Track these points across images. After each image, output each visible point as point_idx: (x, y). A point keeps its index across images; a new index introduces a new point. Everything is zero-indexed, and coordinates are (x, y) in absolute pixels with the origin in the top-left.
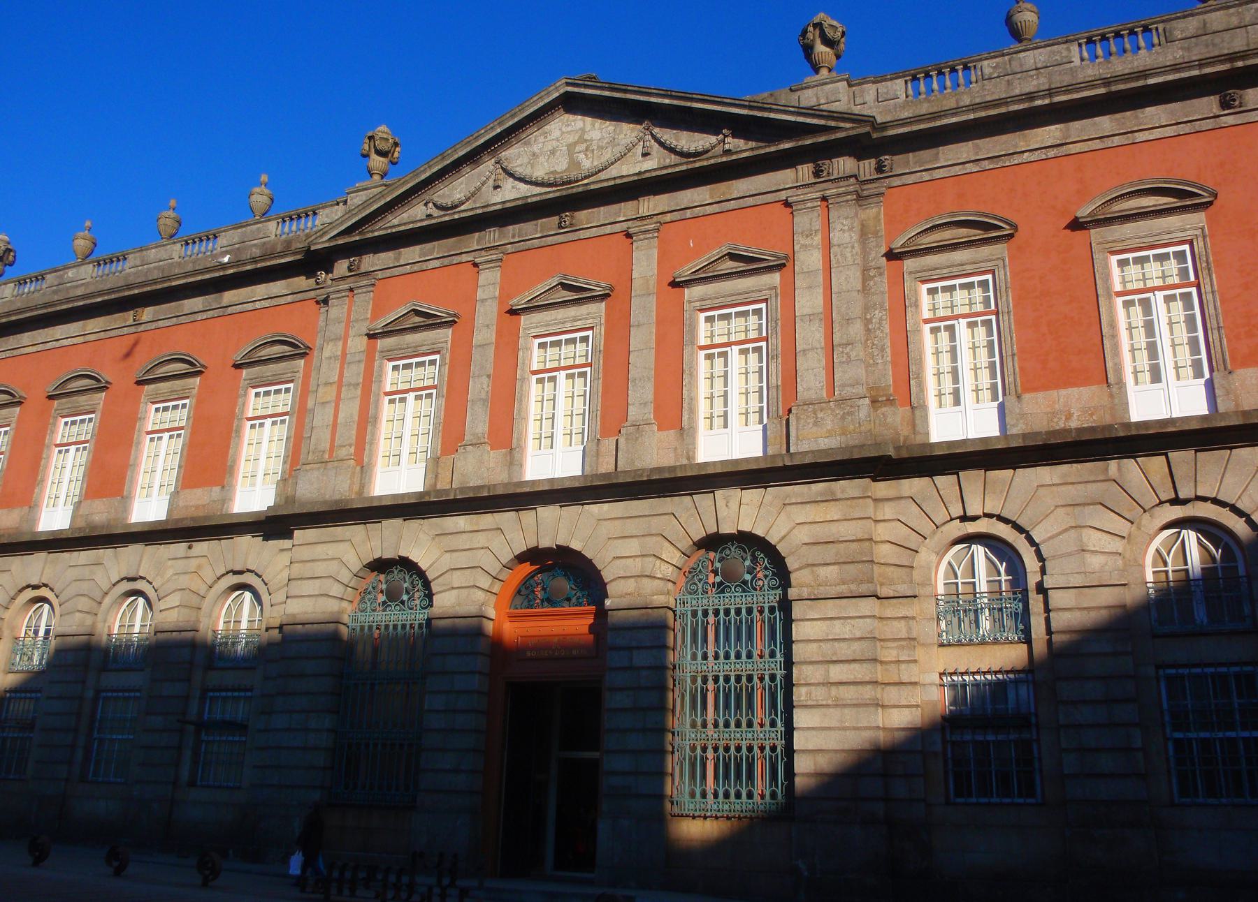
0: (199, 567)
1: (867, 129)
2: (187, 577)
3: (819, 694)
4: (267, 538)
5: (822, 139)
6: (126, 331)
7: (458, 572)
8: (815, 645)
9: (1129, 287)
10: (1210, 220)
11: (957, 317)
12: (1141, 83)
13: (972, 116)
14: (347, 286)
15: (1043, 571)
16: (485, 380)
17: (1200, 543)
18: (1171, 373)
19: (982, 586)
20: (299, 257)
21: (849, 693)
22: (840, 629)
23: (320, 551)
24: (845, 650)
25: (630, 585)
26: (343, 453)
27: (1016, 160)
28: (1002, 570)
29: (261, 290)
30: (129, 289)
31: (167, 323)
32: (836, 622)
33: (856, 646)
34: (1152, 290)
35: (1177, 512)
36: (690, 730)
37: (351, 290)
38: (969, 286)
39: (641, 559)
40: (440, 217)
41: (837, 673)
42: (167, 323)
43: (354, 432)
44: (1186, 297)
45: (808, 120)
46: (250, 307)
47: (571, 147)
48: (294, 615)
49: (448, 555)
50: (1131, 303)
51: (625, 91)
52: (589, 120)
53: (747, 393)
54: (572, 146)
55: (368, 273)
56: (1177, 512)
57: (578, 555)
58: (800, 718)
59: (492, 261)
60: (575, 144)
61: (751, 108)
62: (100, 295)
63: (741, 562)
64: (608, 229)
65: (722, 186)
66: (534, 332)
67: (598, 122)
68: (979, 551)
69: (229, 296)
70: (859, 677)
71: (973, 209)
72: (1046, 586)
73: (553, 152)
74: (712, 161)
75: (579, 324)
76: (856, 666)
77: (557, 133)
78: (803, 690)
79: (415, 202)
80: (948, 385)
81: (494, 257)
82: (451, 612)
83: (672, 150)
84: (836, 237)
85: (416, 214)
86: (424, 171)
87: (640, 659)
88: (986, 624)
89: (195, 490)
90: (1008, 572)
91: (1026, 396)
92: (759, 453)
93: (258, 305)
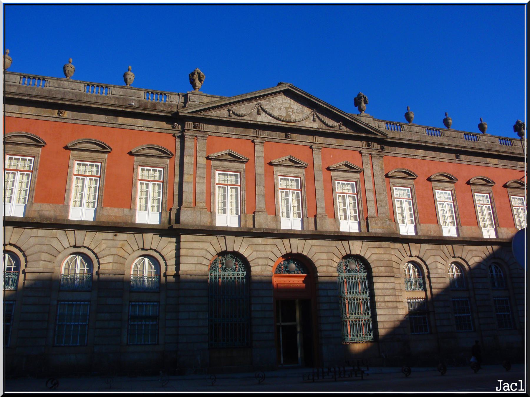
0: (123, 245)
1: (385, 137)
2: (116, 249)
3: (383, 305)
4: (161, 236)
5: (373, 136)
6: (53, 119)
7: (261, 259)
8: (380, 290)
9: (220, 182)
10: (455, 186)
11: (17, 170)
12: (444, 147)
13: (408, 142)
14: (195, 135)
15: (26, 266)
16: (263, 188)
17: (81, 261)
18: (229, 211)
19: (412, 275)
20: (169, 115)
21: (390, 304)
22: (387, 286)
23: (195, 245)
24: (388, 292)
25: (324, 269)
26: (201, 205)
27: (415, 157)
28: (13, 265)
29: (141, 122)
30: (62, 100)
31: (82, 122)
32: (386, 284)
33: (391, 291)
34: (227, 185)
35: (144, 252)
36: (354, 316)
37: (196, 136)
38: (92, 166)
39: (327, 260)
40: (234, 118)
41: (387, 298)
42: (82, 122)
43: (205, 197)
44: (237, 189)
45: (370, 130)
46: (136, 128)
47: (287, 109)
48: (186, 271)
49: (255, 253)
50: (350, 196)
51: (311, 97)
52: (292, 101)
53: (21, 190)
54: (283, 108)
55: (204, 132)
56: (144, 252)
57: (305, 257)
58: (378, 312)
59: (261, 142)
60: (288, 108)
61: (352, 119)
62: (40, 98)
63: (232, 262)
64: (304, 144)
65: (340, 140)
66: (279, 174)
67: (296, 103)
68: (147, 260)
69: (121, 120)
70: (392, 300)
71: (406, 168)
72: (167, 274)
73: (280, 108)
74: (342, 133)
75: (296, 175)
76: (391, 297)
77: (280, 101)
78: (378, 303)
79: (224, 108)
80: (78, 199)
81: (262, 141)
82: (260, 274)
83: (323, 123)
84: (374, 167)
85: (223, 114)
86: (233, 99)
87: (330, 293)
88: (413, 286)
89: (113, 208)
90: (87, 267)
91: (422, 225)
92: (21, 215)
93: (140, 128)
